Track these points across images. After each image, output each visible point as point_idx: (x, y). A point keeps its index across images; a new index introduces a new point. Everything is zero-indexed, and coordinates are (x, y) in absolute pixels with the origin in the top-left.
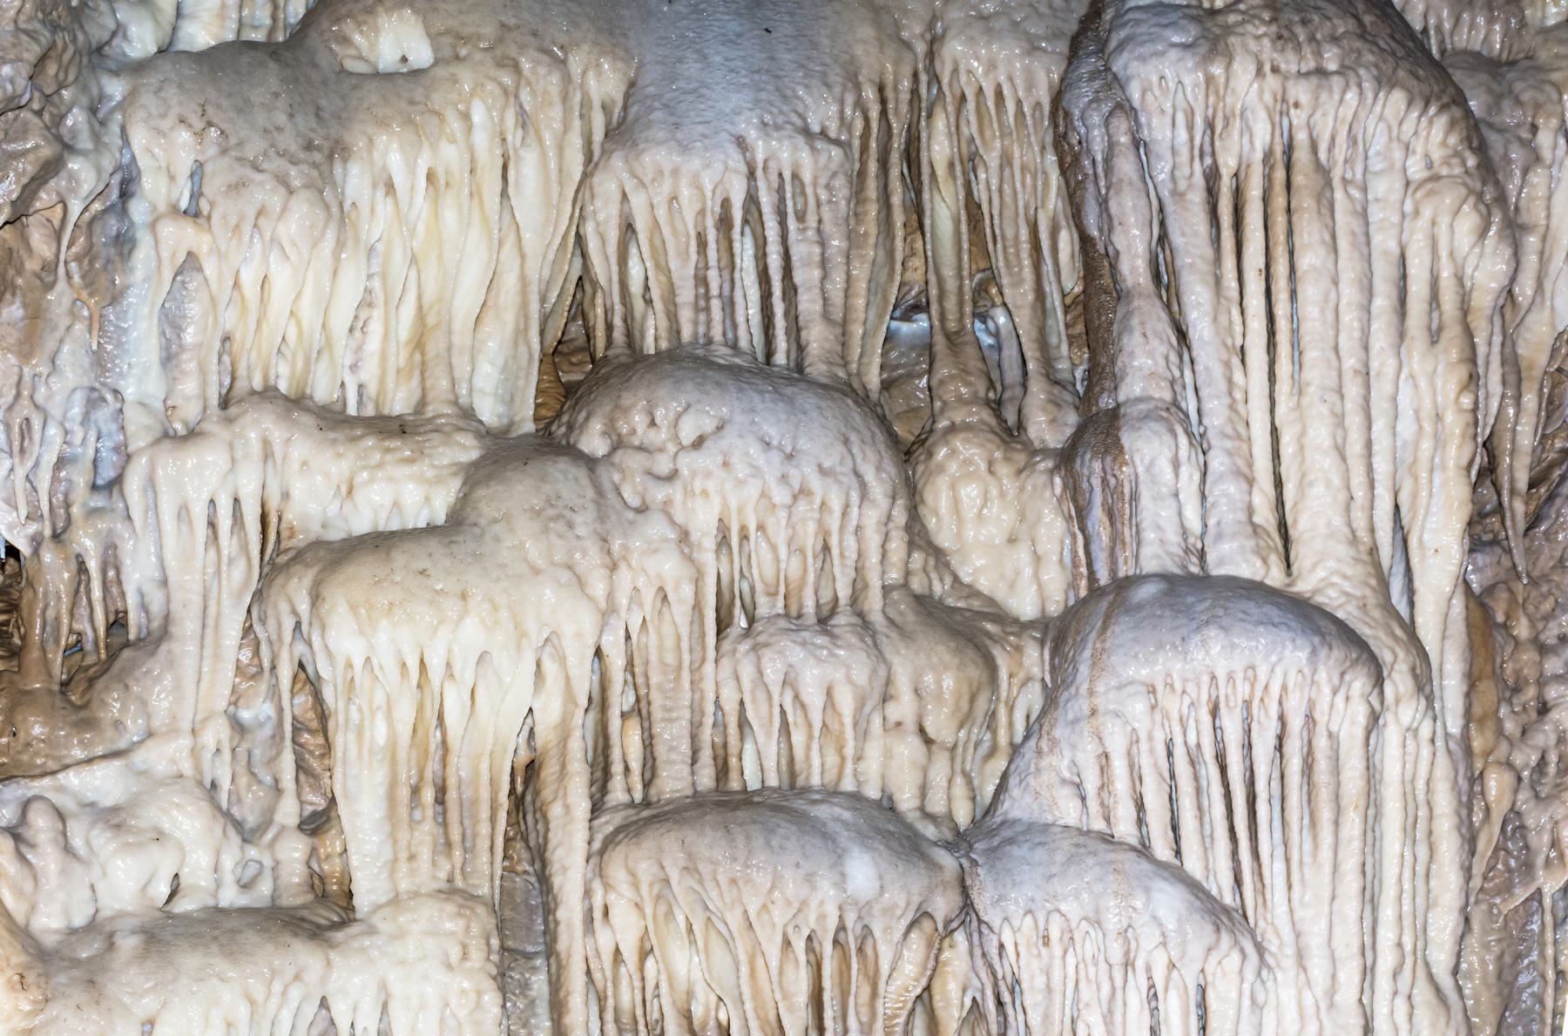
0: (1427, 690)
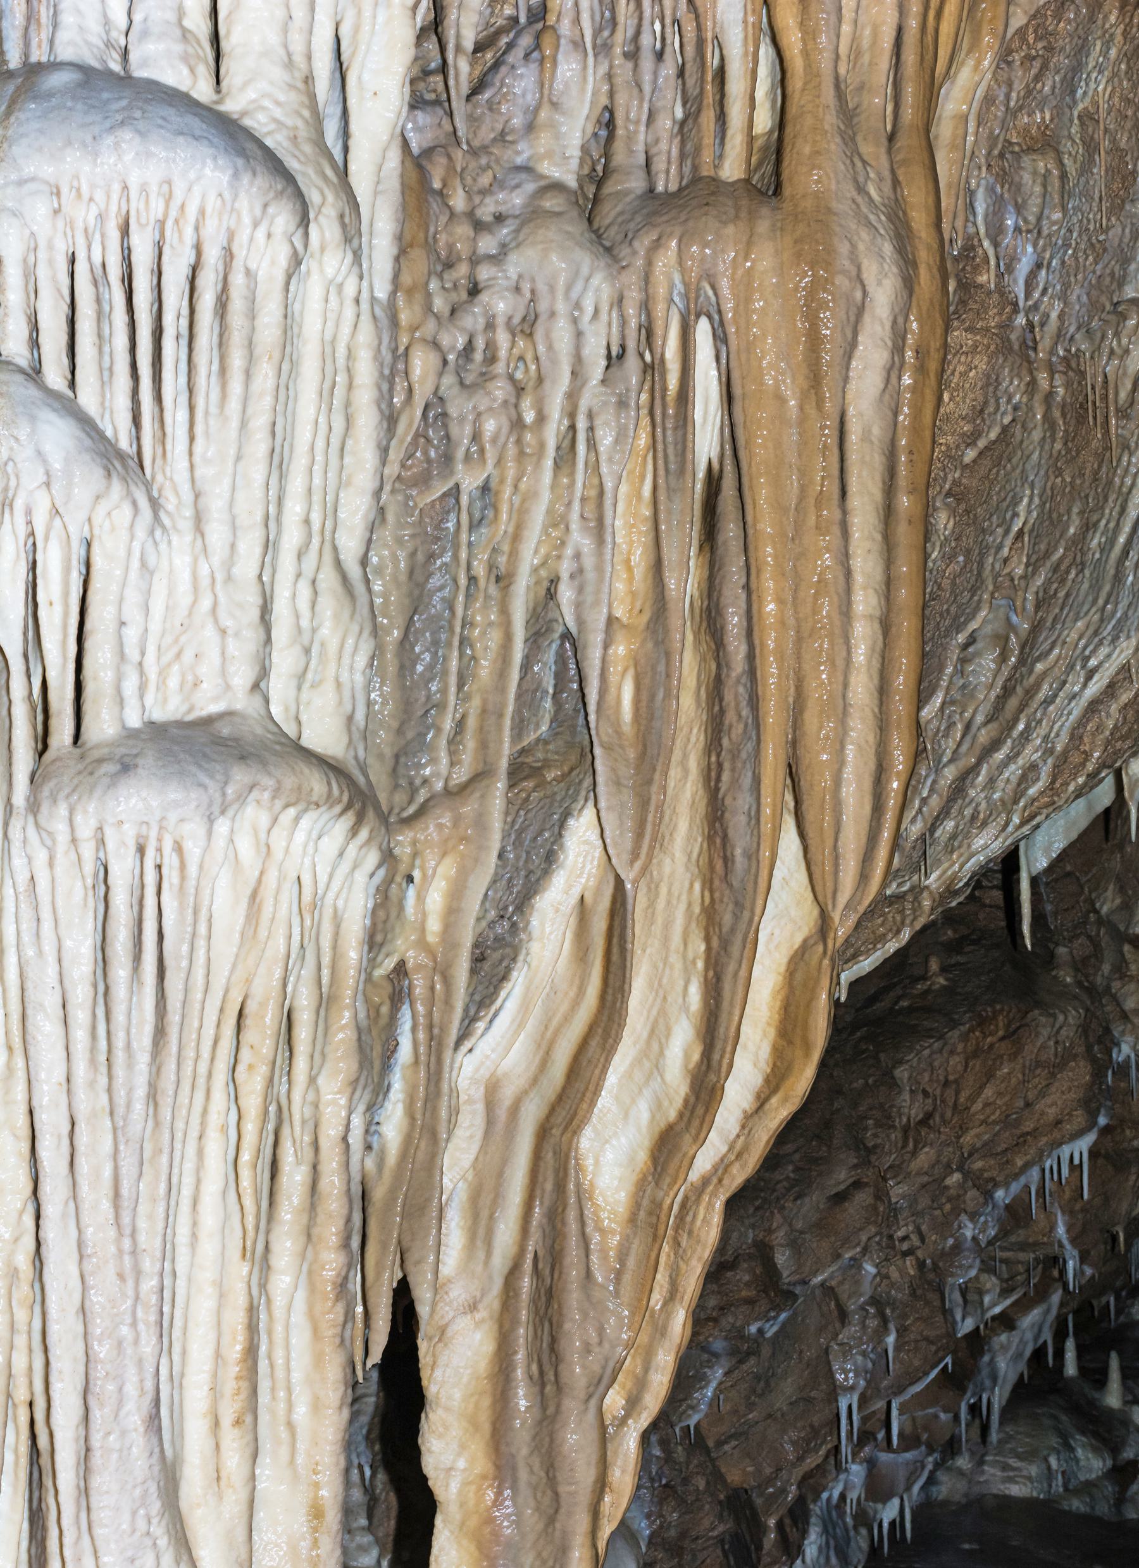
0: (356, 242)
